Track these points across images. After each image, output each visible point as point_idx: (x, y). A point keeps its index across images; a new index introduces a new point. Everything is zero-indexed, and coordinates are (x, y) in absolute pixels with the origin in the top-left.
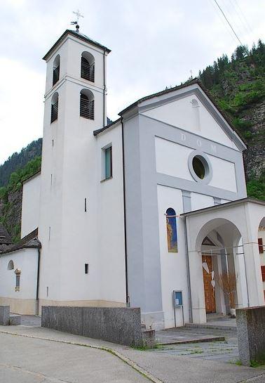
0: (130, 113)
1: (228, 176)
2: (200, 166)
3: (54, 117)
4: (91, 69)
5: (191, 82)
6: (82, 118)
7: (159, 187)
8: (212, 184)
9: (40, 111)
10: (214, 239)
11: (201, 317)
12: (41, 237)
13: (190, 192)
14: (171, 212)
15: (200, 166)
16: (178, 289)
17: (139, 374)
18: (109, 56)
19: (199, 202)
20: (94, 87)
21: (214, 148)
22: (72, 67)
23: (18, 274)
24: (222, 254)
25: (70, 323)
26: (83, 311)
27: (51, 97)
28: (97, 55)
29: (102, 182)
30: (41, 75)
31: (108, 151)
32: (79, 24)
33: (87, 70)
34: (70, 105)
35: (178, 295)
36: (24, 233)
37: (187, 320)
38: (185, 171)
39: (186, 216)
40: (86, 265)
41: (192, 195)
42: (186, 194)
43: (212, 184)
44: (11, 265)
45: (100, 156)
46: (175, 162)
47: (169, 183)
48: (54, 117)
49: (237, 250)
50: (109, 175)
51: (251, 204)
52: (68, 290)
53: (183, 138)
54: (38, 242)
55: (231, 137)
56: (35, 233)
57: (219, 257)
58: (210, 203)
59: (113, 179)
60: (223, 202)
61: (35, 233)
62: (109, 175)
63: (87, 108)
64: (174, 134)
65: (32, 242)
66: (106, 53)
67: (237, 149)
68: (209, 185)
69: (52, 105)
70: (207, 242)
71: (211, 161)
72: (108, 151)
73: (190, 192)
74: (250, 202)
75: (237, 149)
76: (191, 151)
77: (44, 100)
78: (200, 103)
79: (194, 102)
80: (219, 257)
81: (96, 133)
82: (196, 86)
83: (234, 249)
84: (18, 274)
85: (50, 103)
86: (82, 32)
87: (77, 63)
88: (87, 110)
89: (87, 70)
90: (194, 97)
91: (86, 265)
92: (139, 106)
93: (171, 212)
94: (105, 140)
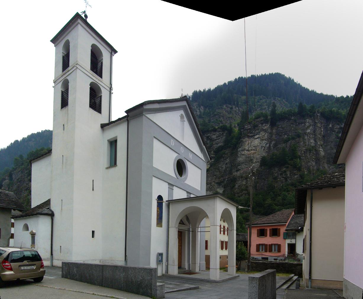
0: (136, 113)
1: (196, 179)
2: (181, 167)
3: (64, 103)
4: (100, 64)
5: (184, 98)
6: (91, 109)
7: (154, 178)
8: (187, 182)
9: (49, 96)
10: (185, 221)
11: (174, 270)
12: (54, 207)
13: (173, 185)
14: (160, 198)
15: (181, 167)
16: (160, 252)
17: (87, 294)
18: (115, 57)
19: (179, 194)
20: (102, 83)
21: (191, 156)
22: (82, 57)
23: (33, 235)
24: (189, 231)
25: (90, 276)
26: (102, 268)
27: (62, 81)
28: (105, 54)
29: (107, 168)
30: (50, 55)
31: (113, 143)
32: (87, 13)
33: (96, 65)
34: (80, 95)
35: (161, 255)
36: (34, 203)
37: (164, 272)
38: (171, 170)
39: (170, 202)
40: (93, 232)
41: (175, 188)
42: (171, 187)
43: (187, 182)
44: (26, 228)
45: (105, 148)
46: (163, 159)
47: (162, 176)
48: (64, 103)
49: (198, 229)
50: (113, 162)
51: (219, 198)
52: (83, 250)
53: (172, 143)
54: (51, 211)
55: (202, 150)
56: (48, 203)
57: (187, 232)
58: (184, 195)
59: (117, 168)
60: (192, 196)
61: (48, 203)
62: (113, 162)
63: (95, 101)
64: (166, 139)
65: (46, 211)
66: (113, 53)
67: (205, 160)
68: (185, 182)
69: (62, 92)
70: (181, 223)
71: (189, 165)
72: (113, 143)
73: (173, 185)
74: (219, 197)
75: (205, 160)
76: (177, 155)
77: (53, 85)
78: (185, 119)
79: (182, 117)
80: (187, 232)
81: (103, 126)
82: (184, 103)
83: (197, 228)
84: (33, 235)
85: (60, 88)
86: (88, 20)
87: (83, 55)
88: (95, 103)
89: (96, 65)
90: (182, 112)
91: (93, 232)
92: (146, 107)
93: (160, 198)
94: (111, 134)
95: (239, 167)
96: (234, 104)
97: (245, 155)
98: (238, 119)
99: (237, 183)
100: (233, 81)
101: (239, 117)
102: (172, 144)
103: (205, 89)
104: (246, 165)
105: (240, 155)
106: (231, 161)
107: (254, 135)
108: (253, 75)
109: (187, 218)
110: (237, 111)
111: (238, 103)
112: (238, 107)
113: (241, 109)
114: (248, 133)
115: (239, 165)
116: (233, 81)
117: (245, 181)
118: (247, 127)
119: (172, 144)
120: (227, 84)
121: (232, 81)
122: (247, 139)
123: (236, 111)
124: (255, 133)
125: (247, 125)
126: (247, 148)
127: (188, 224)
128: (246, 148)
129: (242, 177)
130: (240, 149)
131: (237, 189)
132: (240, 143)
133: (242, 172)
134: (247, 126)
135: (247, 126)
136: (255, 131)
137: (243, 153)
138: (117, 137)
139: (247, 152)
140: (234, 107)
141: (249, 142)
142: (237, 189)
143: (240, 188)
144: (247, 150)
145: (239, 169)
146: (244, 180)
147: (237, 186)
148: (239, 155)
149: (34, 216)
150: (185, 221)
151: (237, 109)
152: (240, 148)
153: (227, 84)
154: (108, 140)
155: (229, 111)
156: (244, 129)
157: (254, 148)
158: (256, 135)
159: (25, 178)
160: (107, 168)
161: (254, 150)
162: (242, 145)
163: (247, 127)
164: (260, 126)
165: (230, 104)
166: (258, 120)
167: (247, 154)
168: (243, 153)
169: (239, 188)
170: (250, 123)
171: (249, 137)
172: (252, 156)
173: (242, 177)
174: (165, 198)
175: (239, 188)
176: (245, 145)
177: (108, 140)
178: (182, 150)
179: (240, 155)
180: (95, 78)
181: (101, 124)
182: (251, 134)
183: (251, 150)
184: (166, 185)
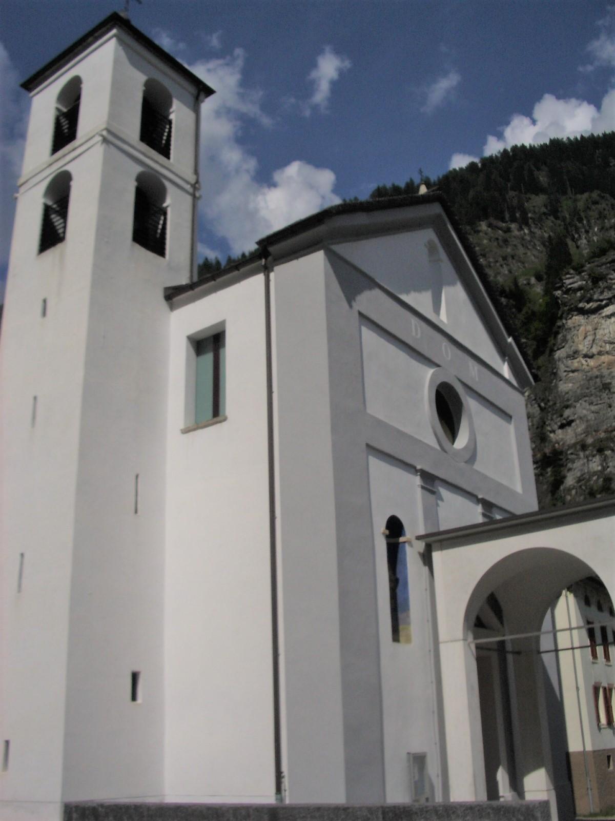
15: (448, 408)
58: (475, 515)
72: (209, 344)
79: (432, 249)
90: (429, 235)
93: (395, 527)
95: (567, 413)
96: (513, 219)
97: (583, 371)
98: (536, 257)
99: (570, 470)
100: (496, 156)
101: (535, 253)
102: (414, 334)
103: (411, 180)
104: (591, 404)
105: (565, 371)
106: (536, 396)
107: (600, 308)
108: (554, 139)
109: (493, 602)
110: (528, 238)
111: (524, 212)
112: (527, 224)
113: (538, 232)
114: (580, 301)
115: (567, 407)
116: (496, 156)
117: (597, 459)
118: (570, 284)
119: (414, 334)
120: (480, 165)
121: (494, 155)
122: (578, 319)
123: (523, 239)
124: (602, 301)
125: (569, 278)
126: (583, 347)
127: (499, 625)
128: (581, 347)
129: (584, 447)
130: (558, 354)
131: (574, 492)
132: (557, 333)
133: (579, 430)
134: (571, 281)
135: (571, 281)
136: (602, 293)
137: (575, 364)
138: (223, 324)
139: (586, 361)
140: (513, 226)
141: (589, 328)
142: (574, 492)
143: (585, 485)
144: (586, 356)
145: (570, 418)
146: (594, 456)
147: (570, 480)
148: (562, 374)
149: (399, 576)
150: (490, 618)
151: (526, 231)
152: (559, 349)
153: (480, 165)
154: (190, 338)
155: (500, 238)
156: (564, 289)
157: (608, 347)
158: (607, 305)
159: (563, 362)
160: (186, 431)
161: (607, 353)
162: (565, 340)
163: (570, 284)
164: (612, 277)
165: (503, 220)
166: (604, 260)
167: (587, 368)
168: (575, 364)
169: (580, 487)
170: (579, 270)
171: (582, 312)
172: (605, 372)
173: (584, 447)
174: (415, 527)
175: (580, 487)
176: (576, 340)
177: (190, 338)
178: (446, 352)
179: (565, 371)
180: (153, 159)
181: (166, 289)
182: (588, 303)
183: (600, 353)
184: (417, 480)
